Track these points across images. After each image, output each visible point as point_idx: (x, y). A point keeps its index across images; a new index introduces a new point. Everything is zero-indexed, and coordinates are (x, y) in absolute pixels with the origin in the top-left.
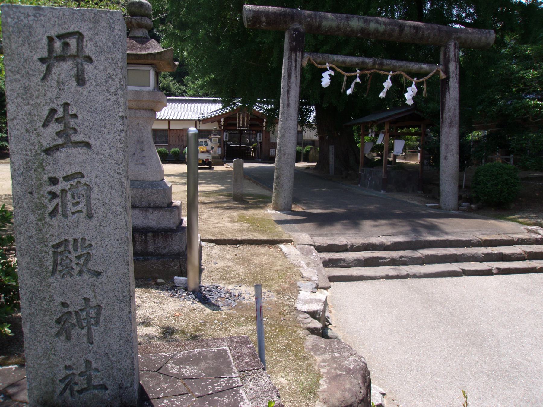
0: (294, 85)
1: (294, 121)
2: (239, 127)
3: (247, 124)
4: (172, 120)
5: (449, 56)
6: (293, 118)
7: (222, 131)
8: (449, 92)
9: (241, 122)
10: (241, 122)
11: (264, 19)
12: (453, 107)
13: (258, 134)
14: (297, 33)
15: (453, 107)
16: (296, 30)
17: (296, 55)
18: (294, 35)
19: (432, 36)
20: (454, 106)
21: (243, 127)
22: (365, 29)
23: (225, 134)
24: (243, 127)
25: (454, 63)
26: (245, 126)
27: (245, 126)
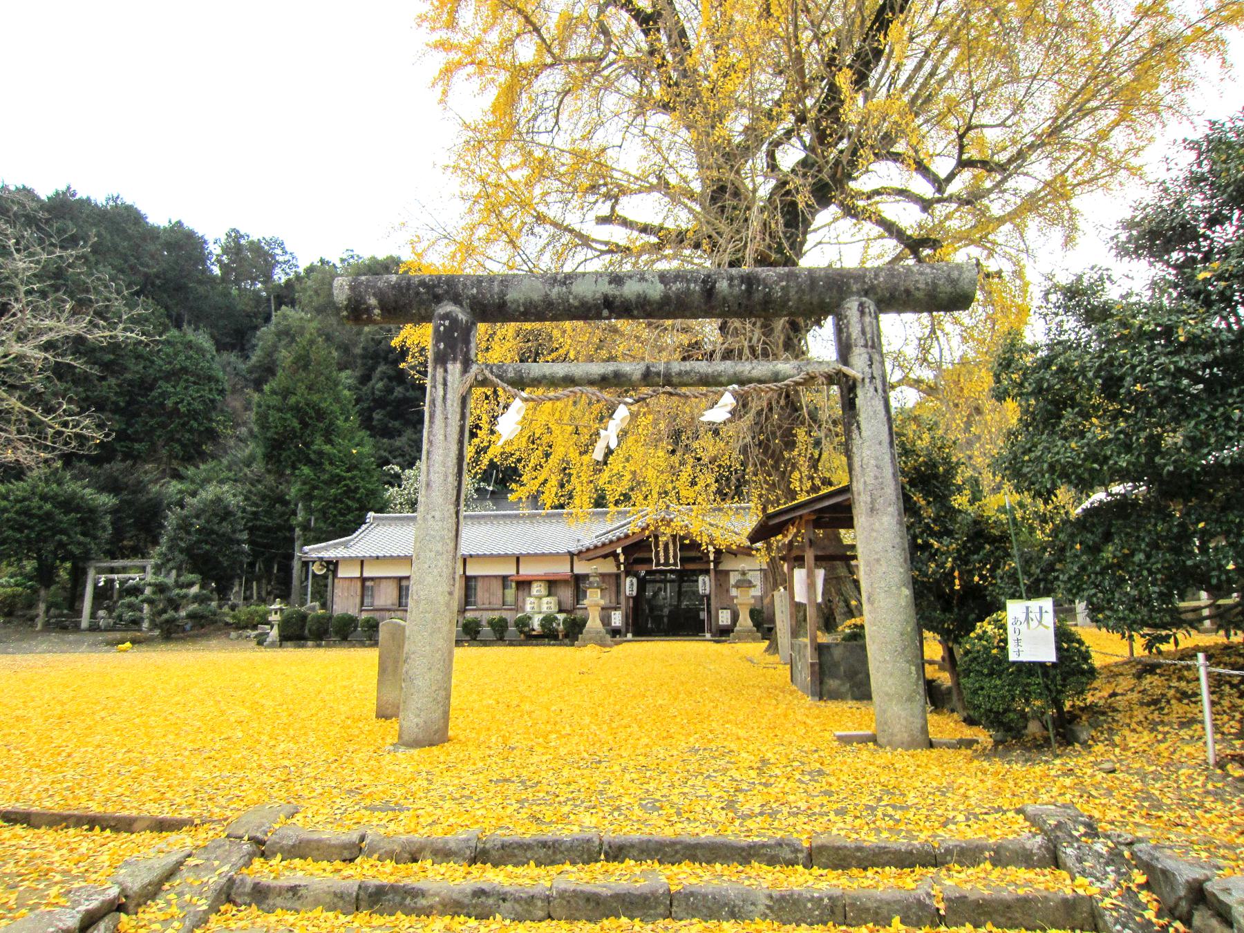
0: (441, 437)
1: (443, 520)
2: (658, 564)
3: (675, 557)
4: (471, 556)
5: (849, 336)
6: (438, 514)
7: (623, 576)
8: (859, 428)
9: (662, 554)
10: (662, 554)
11: (373, 301)
12: (873, 462)
13: (701, 578)
14: (447, 323)
15: (873, 462)
16: (446, 316)
17: (446, 371)
18: (442, 328)
19: (792, 292)
20: (877, 458)
21: (667, 563)
22: (615, 297)
23: (628, 580)
24: (667, 563)
25: (863, 350)
26: (672, 561)
27: (672, 561)
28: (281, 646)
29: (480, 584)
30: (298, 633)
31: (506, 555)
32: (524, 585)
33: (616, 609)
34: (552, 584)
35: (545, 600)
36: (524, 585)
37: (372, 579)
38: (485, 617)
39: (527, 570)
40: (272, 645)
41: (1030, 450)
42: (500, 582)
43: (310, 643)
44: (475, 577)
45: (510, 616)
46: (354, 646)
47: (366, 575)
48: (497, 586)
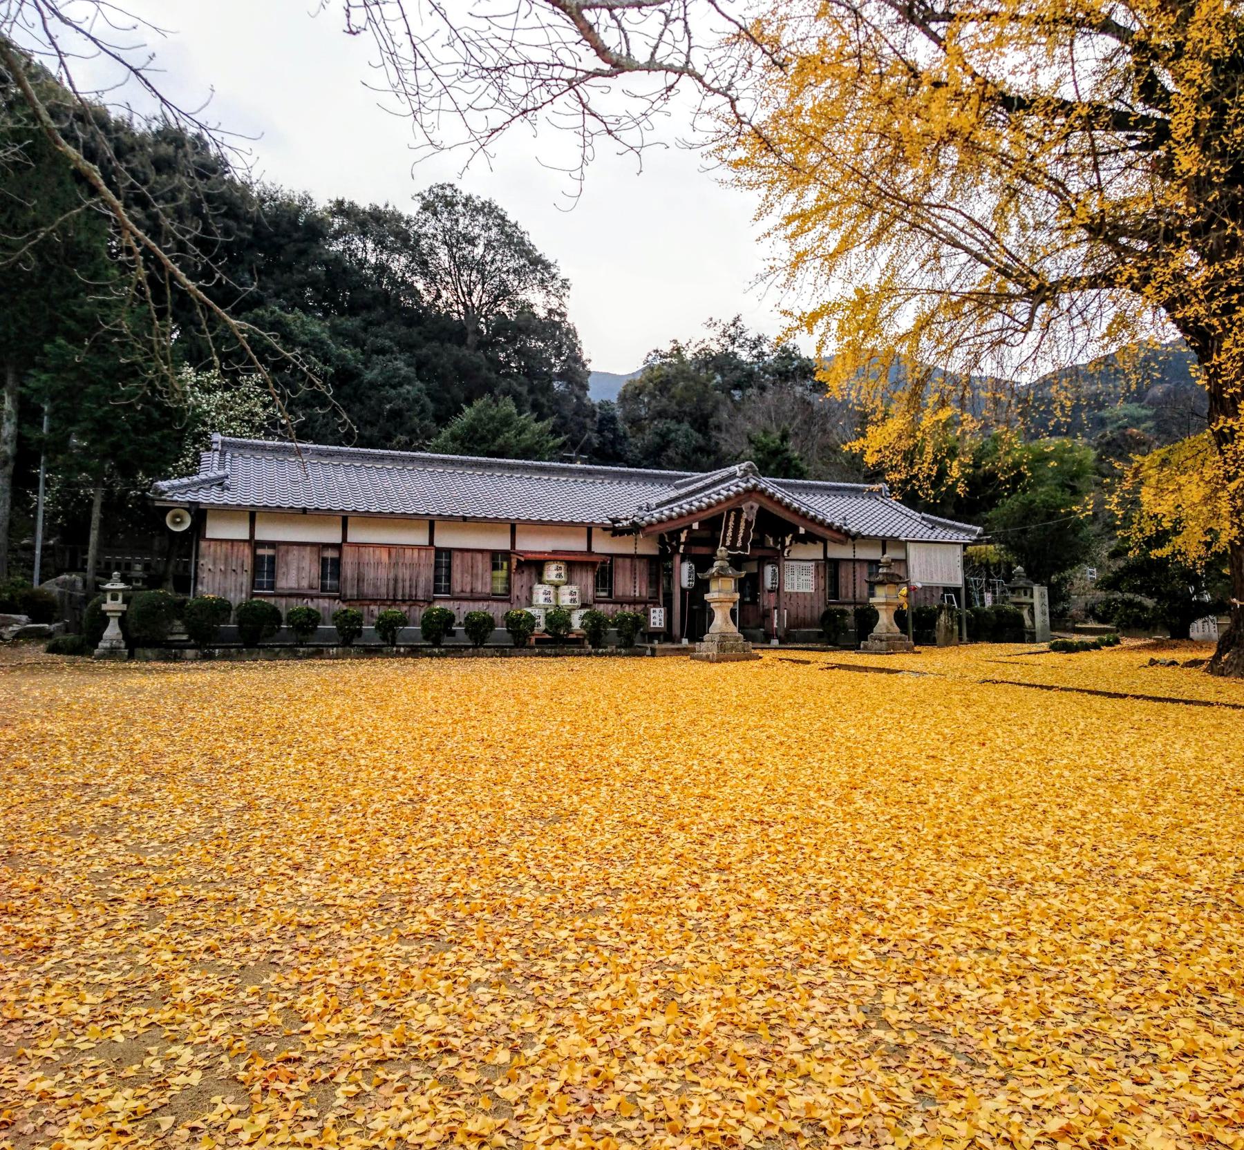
3: (745, 539)
21: (744, 548)
26: (739, 544)
27: (739, 544)
28: (131, 657)
29: (457, 561)
30: (149, 640)
31: (572, 524)
32: (535, 566)
33: (656, 604)
34: (573, 564)
35: (565, 590)
36: (535, 566)
37: (272, 544)
38: (462, 610)
39: (529, 544)
40: (112, 653)
41: (321, 1063)
42: (488, 558)
43: (190, 653)
44: (449, 552)
45: (497, 610)
46: (276, 656)
47: (259, 536)
48: (482, 564)
